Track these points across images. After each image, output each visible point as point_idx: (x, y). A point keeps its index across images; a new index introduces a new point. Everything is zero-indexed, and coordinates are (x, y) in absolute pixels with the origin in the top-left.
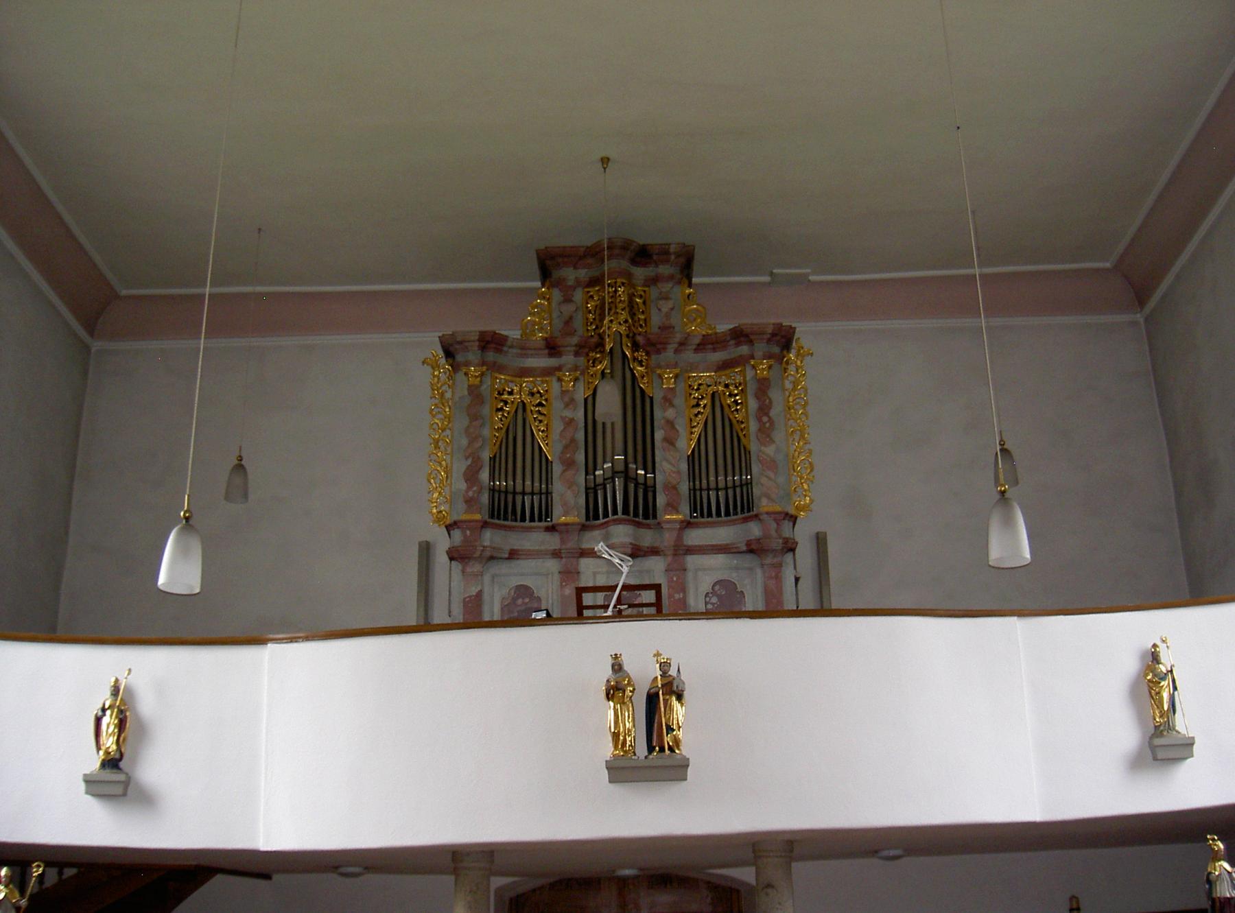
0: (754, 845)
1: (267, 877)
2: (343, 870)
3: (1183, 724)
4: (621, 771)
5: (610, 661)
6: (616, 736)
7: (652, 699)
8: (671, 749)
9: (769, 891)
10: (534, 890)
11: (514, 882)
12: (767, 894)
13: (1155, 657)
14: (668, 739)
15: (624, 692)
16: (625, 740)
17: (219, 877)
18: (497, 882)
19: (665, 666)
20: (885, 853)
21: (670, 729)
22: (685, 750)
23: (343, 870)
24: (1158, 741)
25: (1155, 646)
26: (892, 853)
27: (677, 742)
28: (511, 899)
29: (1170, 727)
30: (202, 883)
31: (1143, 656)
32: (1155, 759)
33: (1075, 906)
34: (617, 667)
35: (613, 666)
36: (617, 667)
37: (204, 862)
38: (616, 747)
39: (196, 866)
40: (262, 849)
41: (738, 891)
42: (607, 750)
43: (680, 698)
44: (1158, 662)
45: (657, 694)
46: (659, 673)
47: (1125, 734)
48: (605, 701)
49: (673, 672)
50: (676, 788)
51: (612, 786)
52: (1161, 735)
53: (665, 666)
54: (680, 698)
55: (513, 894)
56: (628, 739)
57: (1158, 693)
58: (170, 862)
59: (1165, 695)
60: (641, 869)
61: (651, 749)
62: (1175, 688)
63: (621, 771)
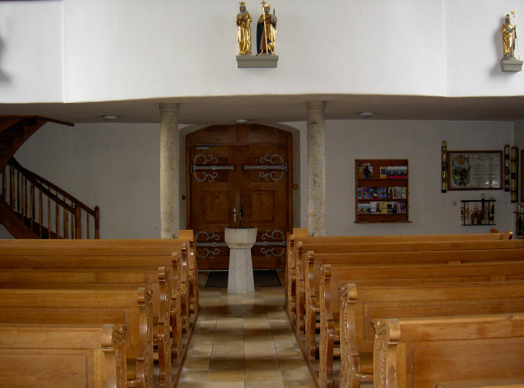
0: (307, 103)
1: (72, 125)
2: (106, 118)
3: (519, 54)
4: (244, 61)
5: (239, 6)
6: (241, 44)
7: (260, 26)
8: (269, 51)
9: (314, 125)
10: (197, 131)
11: (189, 127)
12: (313, 127)
13: (507, 21)
14: (267, 47)
15: (246, 22)
16: (246, 46)
17: (48, 124)
18: (181, 126)
19: (267, 9)
20: (364, 114)
21: (269, 41)
22: (276, 52)
23: (106, 118)
24: (505, 62)
25: (508, 15)
26: (368, 114)
27: (273, 49)
28: (186, 136)
29: (511, 55)
30: (41, 125)
31: (502, 20)
32: (503, 71)
33: (444, 146)
34: (243, 9)
35: (241, 8)
36: (243, 9)
37: (39, 114)
38: (241, 50)
39: (35, 116)
40: (65, 102)
41: (291, 133)
42: (237, 51)
43: (274, 25)
44: (509, 24)
45: (263, 23)
46: (264, 13)
47: (489, 57)
48: (237, 27)
49: (271, 12)
50: (275, 69)
51: (241, 70)
52: (507, 58)
53: (267, 9)
54: (274, 25)
55: (187, 132)
56: (248, 46)
57: (508, 39)
58: (22, 114)
59: (511, 40)
60: (248, 120)
61: (259, 51)
62: (515, 37)
63: (244, 61)
